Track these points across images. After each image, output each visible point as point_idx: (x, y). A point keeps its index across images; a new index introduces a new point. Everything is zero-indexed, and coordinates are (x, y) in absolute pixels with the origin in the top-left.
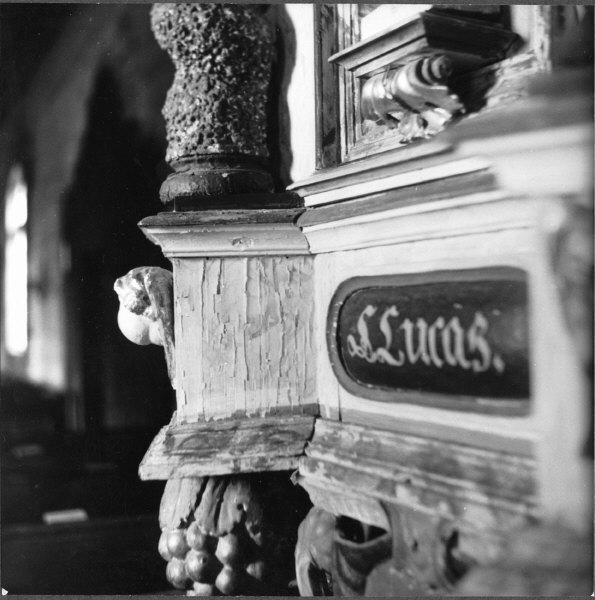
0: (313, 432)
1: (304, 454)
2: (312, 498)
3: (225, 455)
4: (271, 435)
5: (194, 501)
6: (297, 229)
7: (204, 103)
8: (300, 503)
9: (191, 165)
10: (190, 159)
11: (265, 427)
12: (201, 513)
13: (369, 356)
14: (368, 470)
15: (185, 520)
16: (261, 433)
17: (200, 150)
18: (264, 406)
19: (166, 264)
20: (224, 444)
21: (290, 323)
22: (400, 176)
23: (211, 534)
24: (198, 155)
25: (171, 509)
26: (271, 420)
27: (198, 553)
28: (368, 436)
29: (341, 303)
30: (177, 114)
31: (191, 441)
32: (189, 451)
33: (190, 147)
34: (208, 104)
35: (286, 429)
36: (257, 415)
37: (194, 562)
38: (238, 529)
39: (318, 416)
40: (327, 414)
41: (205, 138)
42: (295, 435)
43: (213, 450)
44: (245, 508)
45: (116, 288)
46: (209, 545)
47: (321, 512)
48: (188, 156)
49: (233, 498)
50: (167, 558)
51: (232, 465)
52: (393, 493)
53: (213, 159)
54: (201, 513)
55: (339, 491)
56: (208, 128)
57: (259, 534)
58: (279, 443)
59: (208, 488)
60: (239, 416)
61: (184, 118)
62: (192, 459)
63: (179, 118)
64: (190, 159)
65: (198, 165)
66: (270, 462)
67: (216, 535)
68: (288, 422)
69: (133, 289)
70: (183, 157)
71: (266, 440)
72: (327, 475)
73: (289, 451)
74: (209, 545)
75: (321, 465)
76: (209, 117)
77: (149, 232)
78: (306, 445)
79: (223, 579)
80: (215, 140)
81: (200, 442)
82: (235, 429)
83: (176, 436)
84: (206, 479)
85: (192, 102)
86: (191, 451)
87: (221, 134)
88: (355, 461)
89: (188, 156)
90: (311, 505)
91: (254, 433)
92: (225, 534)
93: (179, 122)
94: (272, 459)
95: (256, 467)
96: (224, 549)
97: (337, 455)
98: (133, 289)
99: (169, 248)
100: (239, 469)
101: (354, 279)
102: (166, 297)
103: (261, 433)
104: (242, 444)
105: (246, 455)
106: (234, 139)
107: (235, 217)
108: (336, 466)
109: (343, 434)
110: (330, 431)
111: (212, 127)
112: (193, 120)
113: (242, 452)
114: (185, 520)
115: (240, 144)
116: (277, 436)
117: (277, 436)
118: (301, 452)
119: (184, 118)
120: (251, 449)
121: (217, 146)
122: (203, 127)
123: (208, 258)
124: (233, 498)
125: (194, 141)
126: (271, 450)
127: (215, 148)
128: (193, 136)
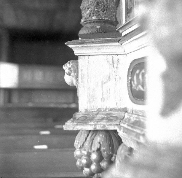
0: (124, 117)
1: (119, 124)
2: (123, 141)
3: (92, 123)
4: (109, 117)
5: (84, 140)
6: (120, 44)
7: (91, 2)
8: (120, 141)
9: (88, 24)
10: (87, 22)
11: (107, 114)
12: (87, 144)
13: (137, 88)
14: (135, 130)
15: (81, 146)
16: (106, 117)
17: (90, 19)
18: (108, 107)
19: (76, 58)
20: (91, 119)
21: (118, 78)
22: (123, 15)
23: (89, 151)
24: (89, 21)
25: (78, 142)
26: (110, 112)
27: (85, 157)
28: (138, 118)
29: (132, 70)
30: (83, 7)
31: (81, 118)
32: (80, 121)
33: (86, 18)
34: (93, 3)
35: (114, 115)
36: (106, 109)
37: (84, 161)
38: (99, 150)
39: (126, 112)
40: (129, 111)
41: (91, 15)
42: (117, 118)
43: (88, 121)
44: (101, 143)
45: (63, 67)
46: (89, 155)
47: (124, 145)
48: (86, 21)
49: (99, 139)
50: (76, 158)
51: (94, 127)
52: (139, 138)
53: (94, 22)
54: (87, 144)
55: (127, 138)
56: (93, 11)
57: (106, 152)
58: (111, 120)
59: (90, 135)
60: (99, 110)
61: (85, 8)
62: (81, 124)
63: (84, 8)
64: (87, 22)
65: (89, 24)
66: (107, 127)
67: (91, 152)
68: (115, 114)
69: (68, 67)
70: (84, 22)
71: (107, 119)
72: (123, 132)
73: (115, 123)
74: (89, 155)
75: (122, 128)
76: (93, 7)
77: (69, 46)
78: (120, 121)
79: (93, 167)
80: (95, 15)
81: (84, 118)
82: (97, 114)
83: (77, 116)
84: (90, 131)
85: (88, 3)
86: (81, 121)
87: (97, 13)
88: (132, 127)
89: (86, 21)
90: (122, 142)
91: (103, 116)
92: (94, 151)
93: (84, 10)
94: (107, 126)
95: (102, 128)
96: (94, 156)
97: (128, 125)
98: (68, 67)
99: (76, 52)
100: (96, 128)
101: (134, 60)
102: (76, 70)
103: (106, 117)
104: (98, 120)
105: (99, 123)
106: (101, 15)
107: (98, 41)
108: (126, 128)
109: (132, 118)
110: (129, 117)
111: (94, 10)
112: (88, 9)
113: (98, 122)
114: (81, 146)
115: (103, 16)
116: (111, 118)
117: (111, 118)
118: (118, 123)
119: (85, 8)
120: (101, 122)
121: (95, 17)
122: (91, 11)
123: (90, 56)
124: (99, 139)
125: (88, 16)
126: (108, 122)
127: (94, 18)
128: (88, 14)
